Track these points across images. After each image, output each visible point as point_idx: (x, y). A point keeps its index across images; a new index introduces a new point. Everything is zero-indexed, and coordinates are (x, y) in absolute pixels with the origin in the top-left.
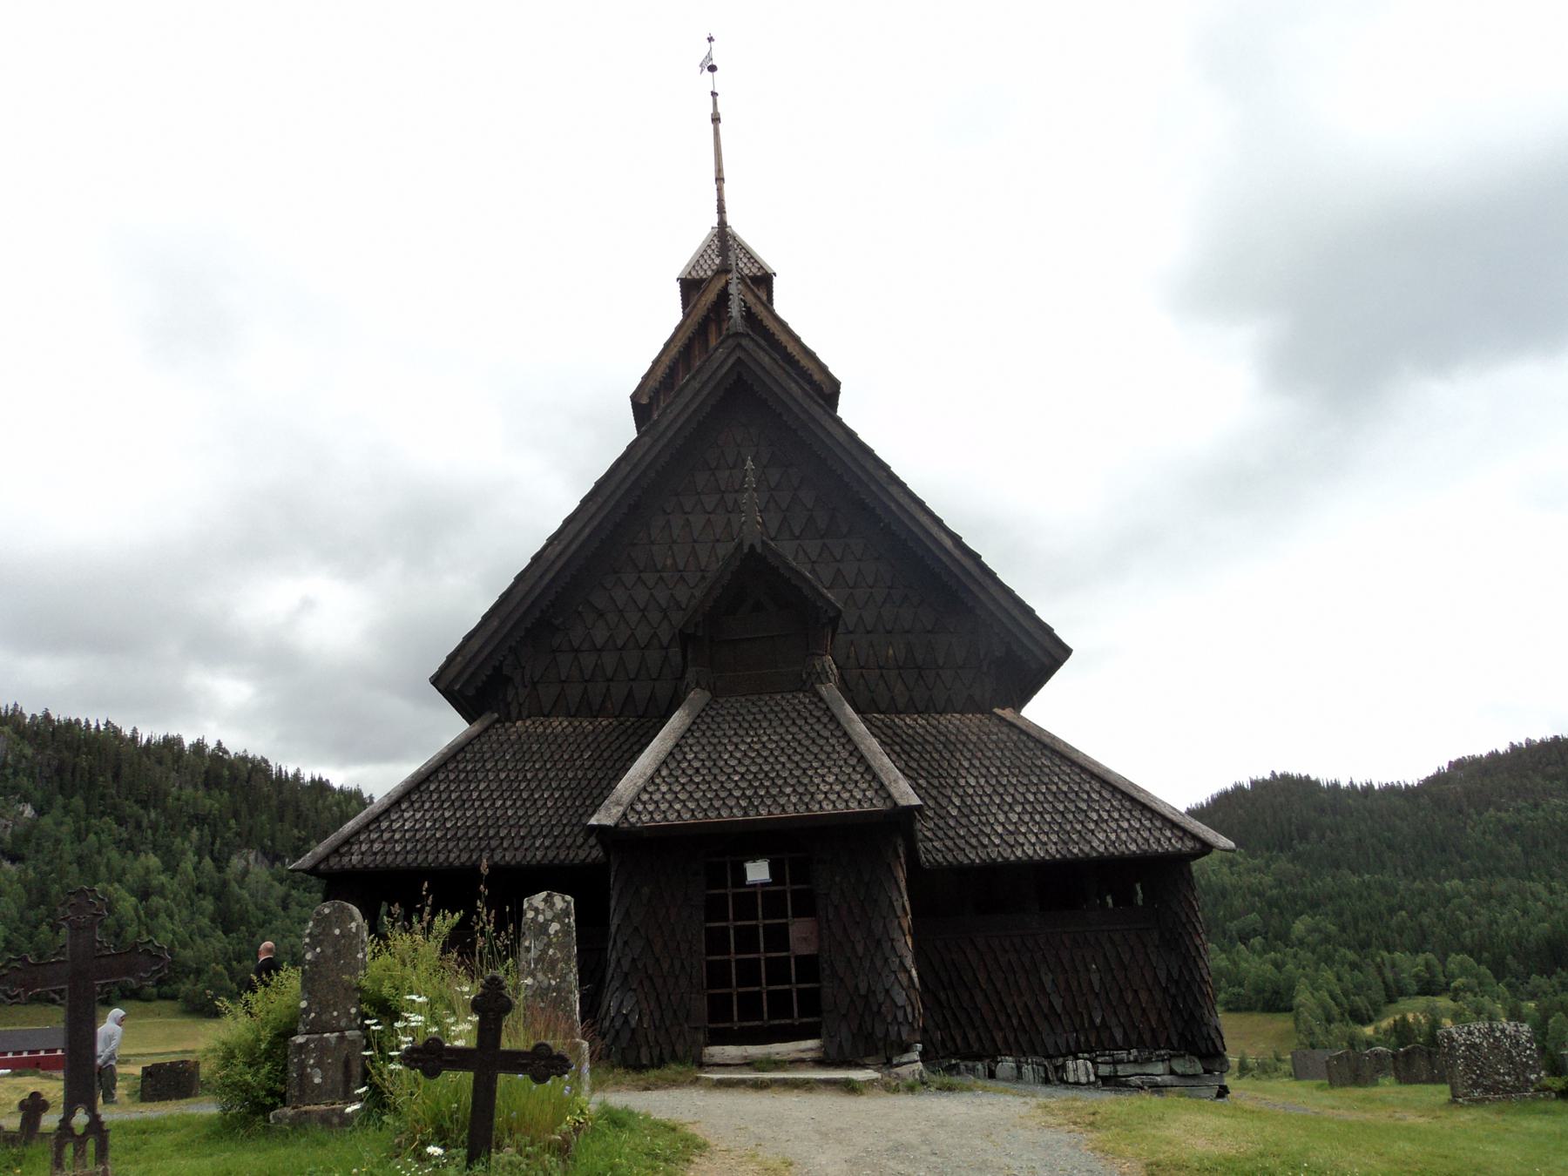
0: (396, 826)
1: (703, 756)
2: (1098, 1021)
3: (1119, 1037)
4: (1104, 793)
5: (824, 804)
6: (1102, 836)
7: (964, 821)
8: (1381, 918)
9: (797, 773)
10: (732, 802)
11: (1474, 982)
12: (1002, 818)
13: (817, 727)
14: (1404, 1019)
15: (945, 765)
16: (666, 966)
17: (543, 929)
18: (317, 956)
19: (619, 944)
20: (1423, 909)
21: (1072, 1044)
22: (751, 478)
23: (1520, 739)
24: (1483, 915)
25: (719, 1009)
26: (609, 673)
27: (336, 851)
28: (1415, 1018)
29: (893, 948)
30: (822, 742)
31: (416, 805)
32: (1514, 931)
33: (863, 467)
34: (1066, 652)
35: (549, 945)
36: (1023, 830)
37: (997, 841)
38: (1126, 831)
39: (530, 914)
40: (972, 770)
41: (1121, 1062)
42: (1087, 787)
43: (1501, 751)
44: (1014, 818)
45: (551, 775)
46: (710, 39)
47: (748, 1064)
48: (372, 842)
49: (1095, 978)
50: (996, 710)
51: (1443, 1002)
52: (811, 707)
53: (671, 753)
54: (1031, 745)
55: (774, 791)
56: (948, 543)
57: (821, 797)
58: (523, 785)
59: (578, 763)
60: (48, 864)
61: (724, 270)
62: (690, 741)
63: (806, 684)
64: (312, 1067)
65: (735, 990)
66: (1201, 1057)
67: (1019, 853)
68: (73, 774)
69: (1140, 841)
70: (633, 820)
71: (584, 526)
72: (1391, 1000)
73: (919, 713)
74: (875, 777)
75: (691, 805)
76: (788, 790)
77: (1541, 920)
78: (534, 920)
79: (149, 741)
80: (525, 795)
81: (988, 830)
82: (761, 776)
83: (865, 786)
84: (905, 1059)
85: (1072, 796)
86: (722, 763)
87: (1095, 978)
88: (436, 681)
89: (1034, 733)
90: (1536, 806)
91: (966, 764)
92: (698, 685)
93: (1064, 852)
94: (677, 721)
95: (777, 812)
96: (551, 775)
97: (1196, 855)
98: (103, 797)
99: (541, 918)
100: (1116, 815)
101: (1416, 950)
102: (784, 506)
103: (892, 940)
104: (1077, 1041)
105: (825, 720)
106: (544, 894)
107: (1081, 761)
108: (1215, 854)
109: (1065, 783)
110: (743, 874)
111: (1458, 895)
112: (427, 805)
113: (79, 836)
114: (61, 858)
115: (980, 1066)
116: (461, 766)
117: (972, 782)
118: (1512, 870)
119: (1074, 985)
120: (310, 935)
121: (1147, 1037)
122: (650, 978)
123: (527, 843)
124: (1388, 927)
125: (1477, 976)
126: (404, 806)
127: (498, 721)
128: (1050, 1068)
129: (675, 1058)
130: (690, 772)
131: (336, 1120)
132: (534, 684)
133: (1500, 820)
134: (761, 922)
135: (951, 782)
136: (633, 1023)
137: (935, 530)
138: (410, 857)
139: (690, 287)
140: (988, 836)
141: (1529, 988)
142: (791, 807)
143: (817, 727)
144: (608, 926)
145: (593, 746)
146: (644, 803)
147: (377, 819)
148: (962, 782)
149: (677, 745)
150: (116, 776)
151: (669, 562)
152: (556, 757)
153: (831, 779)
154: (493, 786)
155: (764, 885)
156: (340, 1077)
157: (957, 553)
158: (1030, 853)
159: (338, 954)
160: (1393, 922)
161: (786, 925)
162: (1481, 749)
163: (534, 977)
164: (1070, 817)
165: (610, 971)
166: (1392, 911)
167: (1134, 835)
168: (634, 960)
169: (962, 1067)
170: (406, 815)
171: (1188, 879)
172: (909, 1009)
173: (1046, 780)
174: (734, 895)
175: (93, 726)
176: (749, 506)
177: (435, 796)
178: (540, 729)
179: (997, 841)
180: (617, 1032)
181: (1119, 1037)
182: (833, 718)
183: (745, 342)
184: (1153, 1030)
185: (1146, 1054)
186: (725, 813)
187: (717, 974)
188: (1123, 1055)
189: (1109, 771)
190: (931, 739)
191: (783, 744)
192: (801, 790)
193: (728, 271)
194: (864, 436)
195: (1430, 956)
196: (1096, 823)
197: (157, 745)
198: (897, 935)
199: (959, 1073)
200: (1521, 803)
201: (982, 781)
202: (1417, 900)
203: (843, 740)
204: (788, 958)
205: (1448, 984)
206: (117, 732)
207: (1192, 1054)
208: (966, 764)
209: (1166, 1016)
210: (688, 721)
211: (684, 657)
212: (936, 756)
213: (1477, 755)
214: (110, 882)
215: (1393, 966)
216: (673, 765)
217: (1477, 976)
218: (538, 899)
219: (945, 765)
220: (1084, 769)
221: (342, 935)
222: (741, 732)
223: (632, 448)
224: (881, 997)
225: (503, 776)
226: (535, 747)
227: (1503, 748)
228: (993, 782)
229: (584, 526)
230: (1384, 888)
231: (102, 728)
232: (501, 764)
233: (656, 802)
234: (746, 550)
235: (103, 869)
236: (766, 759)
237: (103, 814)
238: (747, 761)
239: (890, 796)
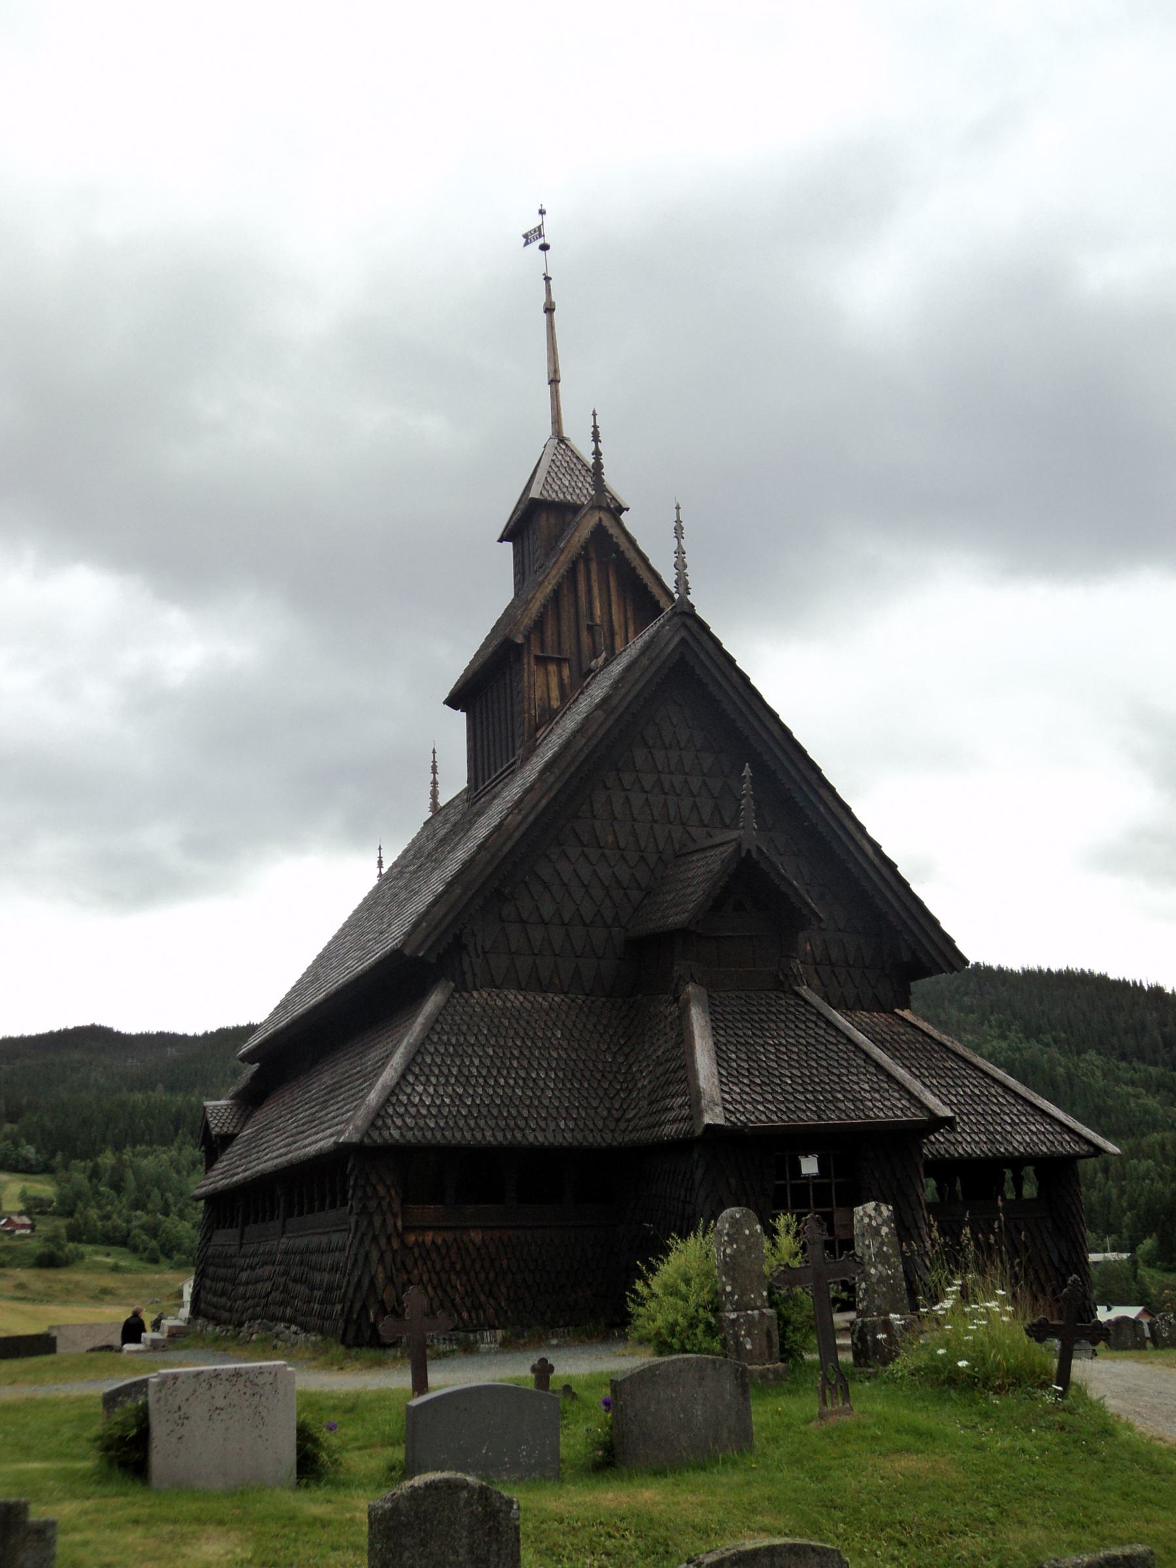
17: (876, 1231)
18: (735, 1251)
35: (882, 1244)
46: (542, 212)
50: (897, 1010)
56: (869, 850)
63: (783, 985)
64: (744, 1336)
67: (961, 1151)
78: (869, 1224)
94: (698, 1020)
106: (872, 1204)
120: (727, 1234)
131: (771, 1376)
137: (858, 837)
155: (814, 1178)
156: (765, 1343)
157: (876, 861)
159: (749, 1248)
163: (876, 1268)
174: (792, 1186)
221: (751, 1234)
234: (743, 854)
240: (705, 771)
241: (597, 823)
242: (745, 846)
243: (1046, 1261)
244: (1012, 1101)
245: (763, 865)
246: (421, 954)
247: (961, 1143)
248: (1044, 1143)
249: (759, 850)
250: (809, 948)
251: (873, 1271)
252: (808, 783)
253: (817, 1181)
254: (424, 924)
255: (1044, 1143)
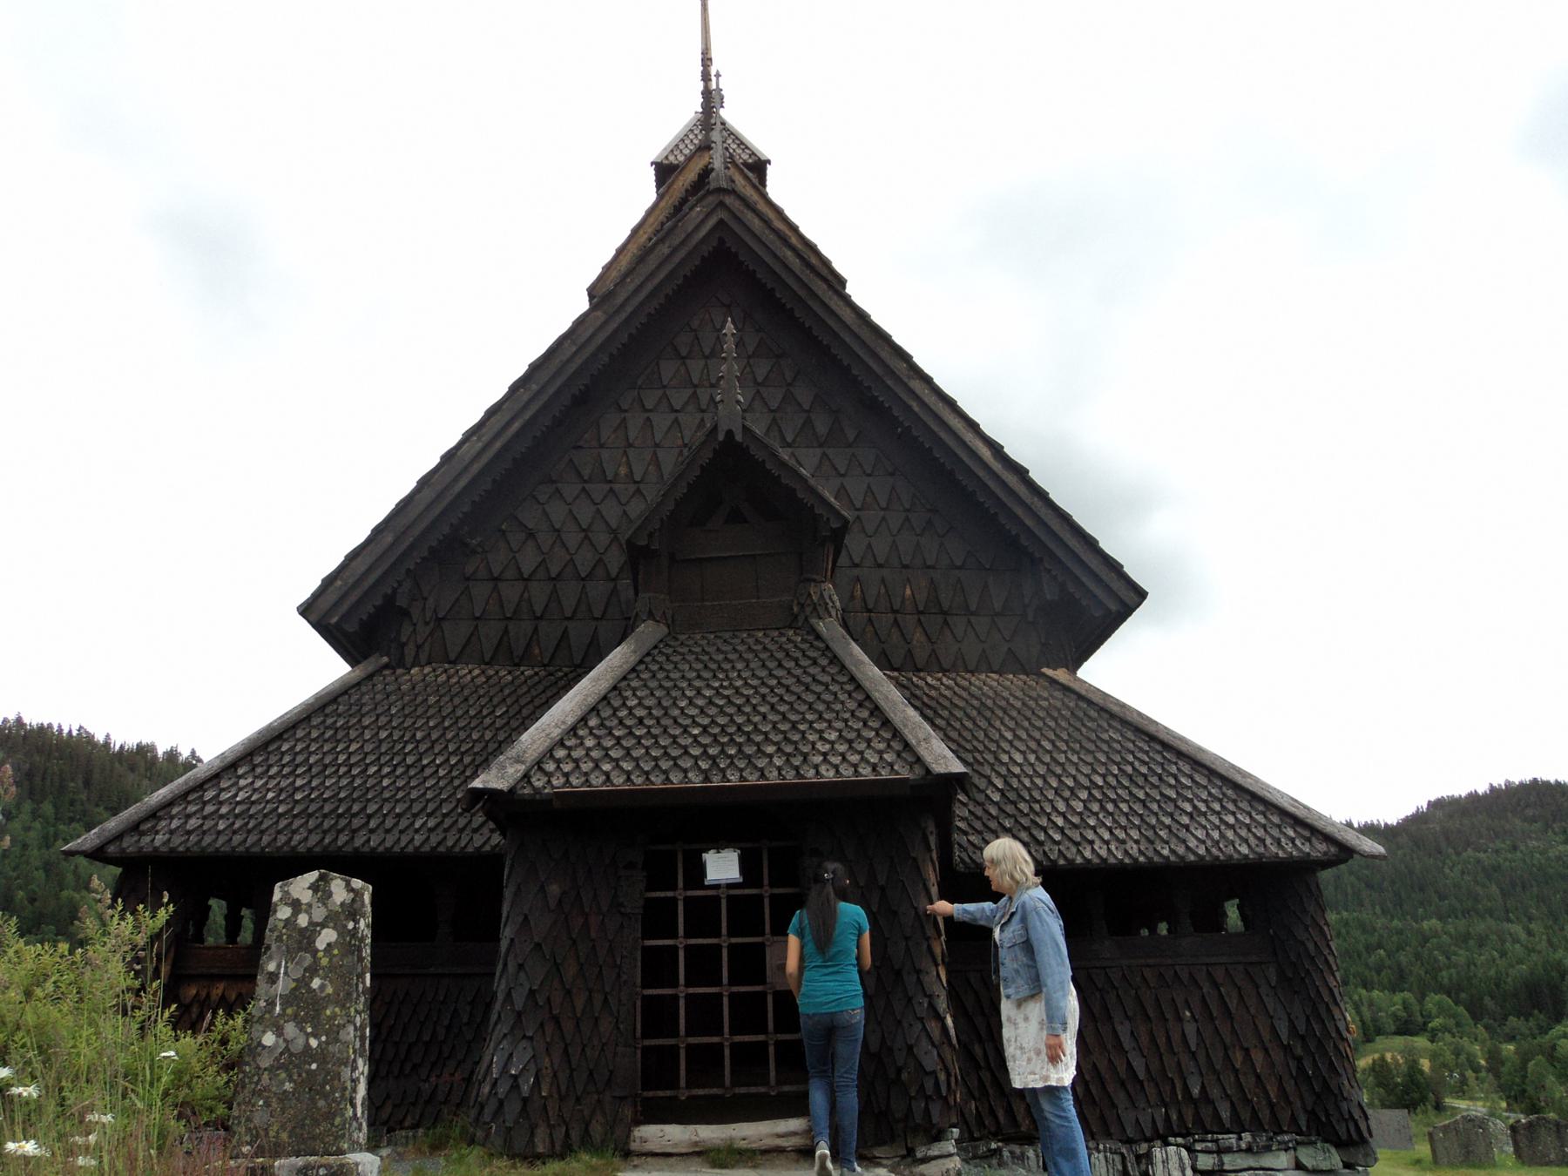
0: (225, 796)
1: (649, 702)
2: (1196, 1091)
3: (1225, 1114)
4: (1197, 778)
5: (823, 769)
6: (1200, 834)
7: (1009, 809)
8: (1359, 956)
9: (784, 727)
10: (686, 763)
11: (1452, 1022)
12: (1061, 806)
13: (812, 670)
14: (1383, 1059)
15: (981, 735)
16: (579, 1004)
17: (306, 939)
19: (511, 968)
20: (1400, 948)
21: (1160, 1125)
22: (729, 345)
23: (1499, 781)
24: (1461, 957)
25: (658, 1069)
26: (538, 610)
27: (135, 828)
28: (1393, 1058)
29: (920, 982)
30: (819, 689)
31: (259, 770)
32: (1492, 972)
33: (875, 355)
34: (1141, 595)
35: (313, 971)
36: (1092, 822)
37: (1057, 837)
38: (1232, 827)
39: (284, 913)
40: (1017, 743)
41: (1229, 1150)
42: (1173, 769)
43: (1481, 791)
44: (1079, 807)
45: (449, 735)
47: (699, 1154)
48: (189, 816)
49: (1190, 1029)
51: (1421, 1042)
52: (805, 646)
53: (605, 698)
54: (1093, 714)
55: (749, 750)
56: (986, 453)
57: (818, 759)
58: (409, 747)
59: (487, 721)
60: (14, 870)
61: (705, 147)
62: (634, 684)
63: (798, 619)
65: (684, 1041)
66: (1340, 1145)
67: (1088, 854)
68: (43, 779)
69: (1253, 841)
70: (538, 784)
71: (513, 420)
72: (1368, 1039)
73: (944, 671)
74: (896, 734)
75: (627, 766)
76: (770, 749)
77: (1520, 962)
79: (122, 747)
80: (409, 760)
81: (1043, 822)
82: (732, 730)
83: (882, 746)
84: (934, 1152)
85: (1154, 780)
86: (676, 712)
87: (1190, 1029)
88: (306, 610)
89: (1096, 699)
90: (1515, 848)
91: (1009, 735)
92: (651, 616)
93: (1150, 853)
94: (617, 659)
95: (753, 779)
96: (449, 735)
97: (1325, 864)
98: (72, 803)
99: (303, 920)
100: (1217, 807)
101: (1394, 988)
102: (774, 405)
103: (918, 972)
104: (1167, 1118)
105: (824, 662)
106: (313, 876)
107: (1162, 736)
108: (1354, 862)
109: (1144, 763)
110: (701, 869)
111: (1436, 935)
112: (273, 771)
113: (47, 842)
114: (28, 863)
115: (1031, 1153)
116: (329, 721)
117: (1019, 758)
118: (1491, 912)
119: (1162, 1041)
121: (1265, 1114)
122: (556, 1020)
123: (404, 823)
124: (1367, 965)
125: (1454, 1016)
126: (240, 771)
127: (386, 666)
128: (1131, 1158)
129: (587, 1143)
130: (629, 722)
132: (439, 620)
133: (1478, 861)
134: (725, 941)
135: (990, 758)
136: (525, 1089)
137: (969, 437)
138: (237, 839)
139: (664, 172)
140: (1045, 830)
141: (1507, 1029)
142: (774, 771)
143: (812, 670)
144: (499, 940)
145: (509, 701)
146: (558, 761)
147: (201, 786)
148: (1005, 758)
149: (615, 688)
150: (87, 783)
151: (623, 471)
152: (459, 712)
153: (833, 736)
154: (368, 747)
155: (731, 886)
157: (996, 466)
158: (1103, 853)
160: (1372, 960)
161: (762, 945)
162: (1460, 789)
163: (279, 1032)
164: (1155, 807)
165: (497, 1006)
166: (1370, 949)
167: (1243, 833)
168: (532, 992)
169: (1006, 1154)
170: (242, 782)
171: (1316, 894)
172: (942, 1077)
173: (1117, 758)
175: (66, 731)
176: (730, 382)
177: (287, 759)
178: (443, 678)
179: (1057, 837)
180: (501, 1103)
181: (1225, 1114)
182: (835, 660)
183: (729, 200)
184: (1271, 1106)
185: (1262, 1140)
186: (676, 778)
187: (658, 1016)
188: (1232, 1139)
189: (1200, 749)
190: (962, 704)
191: (764, 690)
192: (789, 749)
193: (709, 148)
194: (877, 318)
195: (1407, 994)
196: (1191, 815)
197: (130, 752)
198: (926, 964)
199: (1001, 1164)
200: (1499, 844)
201: (1032, 758)
202: (1395, 938)
203: (848, 687)
204: (763, 995)
205: (1425, 1024)
206: (90, 739)
207: (1326, 1141)
208: (1009, 735)
209: (1290, 1086)
210: (633, 659)
211: (635, 580)
212: (969, 724)
213: (1456, 794)
214: (77, 889)
215: (1371, 1004)
216: (607, 712)
217: (1454, 1016)
218: (302, 886)
219: (981, 735)
220: (1166, 746)
222: (706, 675)
223: (580, 323)
224: (900, 1058)
225: (383, 734)
226: (432, 700)
227: (1482, 789)
228: (1047, 759)
229: (513, 420)
230: (1363, 927)
231: (75, 733)
232: (383, 720)
233: (576, 761)
234: (721, 437)
235: (70, 878)
236: (739, 708)
237: (72, 820)
238: (712, 711)
239: (919, 760)
240: (760, 380)
241: (605, 454)
242: (723, 429)
243: (1266, 1036)
244: (1204, 782)
245: (753, 450)
246: (334, 620)
247: (1091, 843)
248: (1246, 841)
249: (745, 429)
250: (908, 592)
251: (269, 1039)
252: (892, 373)
253: (733, 892)
254: (339, 583)
255: (1246, 841)
